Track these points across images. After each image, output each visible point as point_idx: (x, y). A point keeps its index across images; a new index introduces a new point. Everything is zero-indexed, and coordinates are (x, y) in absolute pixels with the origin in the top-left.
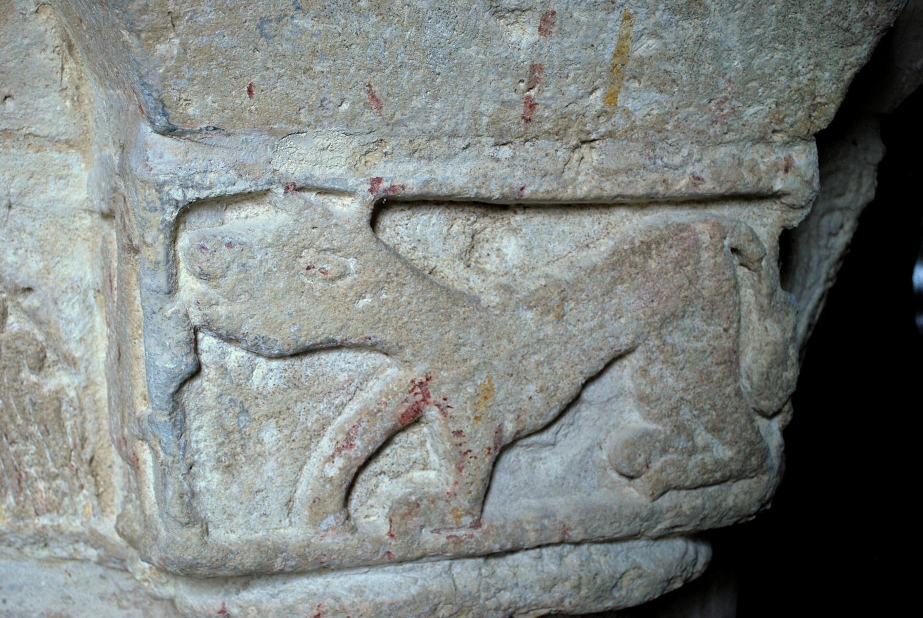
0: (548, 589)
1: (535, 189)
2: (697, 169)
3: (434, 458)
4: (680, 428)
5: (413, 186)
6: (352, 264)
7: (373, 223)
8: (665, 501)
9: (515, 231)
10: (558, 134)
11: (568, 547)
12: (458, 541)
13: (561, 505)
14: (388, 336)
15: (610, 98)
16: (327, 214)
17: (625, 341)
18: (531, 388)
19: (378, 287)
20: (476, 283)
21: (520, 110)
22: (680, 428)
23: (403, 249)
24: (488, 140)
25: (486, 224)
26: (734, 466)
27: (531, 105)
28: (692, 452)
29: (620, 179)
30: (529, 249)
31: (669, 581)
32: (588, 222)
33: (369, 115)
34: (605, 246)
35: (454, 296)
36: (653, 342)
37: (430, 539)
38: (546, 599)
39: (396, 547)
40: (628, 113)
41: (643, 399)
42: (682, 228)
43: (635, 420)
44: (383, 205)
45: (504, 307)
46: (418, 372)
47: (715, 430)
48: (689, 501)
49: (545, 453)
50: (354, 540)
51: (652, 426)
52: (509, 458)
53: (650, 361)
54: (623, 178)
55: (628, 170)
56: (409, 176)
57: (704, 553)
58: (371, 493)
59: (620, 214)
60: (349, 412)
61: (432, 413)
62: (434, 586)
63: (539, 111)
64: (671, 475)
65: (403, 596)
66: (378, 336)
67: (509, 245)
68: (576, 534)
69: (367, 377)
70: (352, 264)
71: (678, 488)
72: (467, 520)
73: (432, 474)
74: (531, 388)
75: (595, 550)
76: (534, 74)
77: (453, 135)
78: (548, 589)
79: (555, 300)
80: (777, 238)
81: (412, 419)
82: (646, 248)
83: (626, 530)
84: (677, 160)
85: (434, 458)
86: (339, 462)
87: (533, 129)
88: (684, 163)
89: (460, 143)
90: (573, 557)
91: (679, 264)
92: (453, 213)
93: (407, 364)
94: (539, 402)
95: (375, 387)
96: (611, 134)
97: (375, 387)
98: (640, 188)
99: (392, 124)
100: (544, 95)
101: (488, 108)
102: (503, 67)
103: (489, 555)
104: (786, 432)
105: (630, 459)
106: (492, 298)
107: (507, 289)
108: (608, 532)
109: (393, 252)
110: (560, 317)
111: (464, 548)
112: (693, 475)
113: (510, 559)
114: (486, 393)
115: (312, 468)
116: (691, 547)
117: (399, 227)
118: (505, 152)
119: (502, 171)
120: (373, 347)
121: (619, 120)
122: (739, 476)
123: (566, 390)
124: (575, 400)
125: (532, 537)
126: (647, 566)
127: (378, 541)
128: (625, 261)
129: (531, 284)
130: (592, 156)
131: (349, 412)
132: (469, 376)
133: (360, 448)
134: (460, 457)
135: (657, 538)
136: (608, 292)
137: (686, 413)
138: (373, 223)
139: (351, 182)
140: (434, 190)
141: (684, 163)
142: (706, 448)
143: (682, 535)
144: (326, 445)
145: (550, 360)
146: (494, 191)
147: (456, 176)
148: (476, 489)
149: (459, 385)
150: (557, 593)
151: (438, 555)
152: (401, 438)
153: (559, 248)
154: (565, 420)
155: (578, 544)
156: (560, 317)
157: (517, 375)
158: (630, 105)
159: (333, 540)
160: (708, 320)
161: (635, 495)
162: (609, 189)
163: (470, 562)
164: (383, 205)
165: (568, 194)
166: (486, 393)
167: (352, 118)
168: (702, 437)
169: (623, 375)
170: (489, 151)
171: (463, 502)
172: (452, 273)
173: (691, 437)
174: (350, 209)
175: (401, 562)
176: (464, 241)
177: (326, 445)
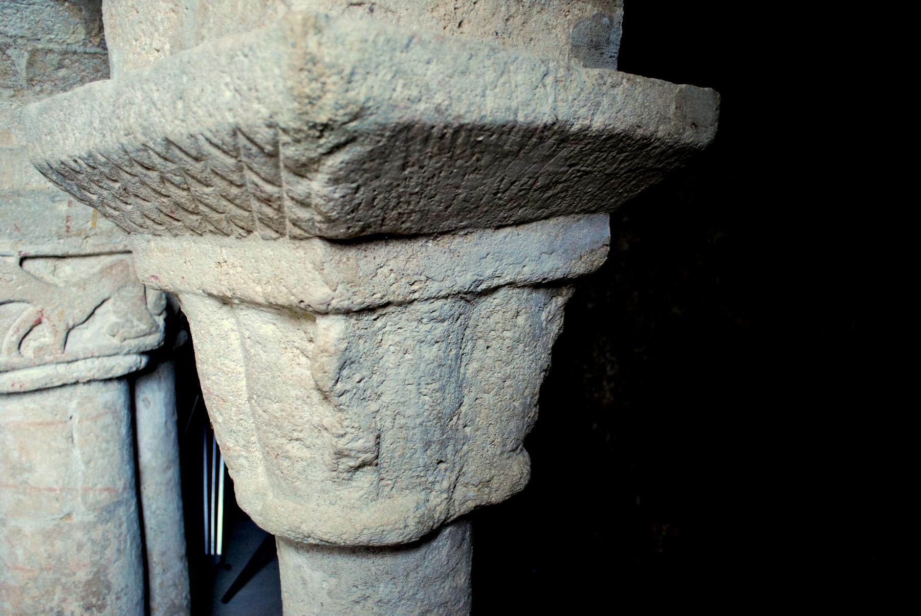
0: (90, 371)
1: (72, 252)
2: (125, 243)
3: (47, 334)
4: (127, 320)
5: (32, 253)
6: (14, 277)
7: (21, 264)
8: (126, 343)
9: (69, 264)
10: (78, 235)
11: (95, 359)
12: (57, 358)
13: (90, 346)
14: (28, 298)
15: (94, 224)
16: (5, 262)
17: (106, 296)
18: (77, 311)
19: (23, 283)
20: (56, 280)
21: (65, 229)
22: (127, 320)
23: (32, 272)
24: (55, 238)
25: (59, 263)
26: (147, 331)
27: (68, 227)
28: (133, 327)
29: (562, 70)
30: (73, 269)
31: (131, 368)
32: (92, 260)
33: (16, 233)
34: (99, 267)
35: (48, 284)
36: (116, 295)
37: (48, 358)
38: (89, 375)
39: (37, 361)
40: (100, 228)
41: (115, 312)
42: (122, 261)
43: (113, 319)
44: (22, 260)
45: (65, 287)
46: (39, 308)
47: (140, 320)
48: (134, 343)
49: (85, 331)
50: (22, 360)
51: (118, 320)
52: (72, 333)
53: (116, 301)
54: (101, 247)
55: (102, 244)
56: (31, 250)
57: (144, 360)
58: (27, 346)
59: (102, 257)
60: (18, 321)
61: (44, 320)
62: (51, 372)
63: (71, 229)
64: (126, 335)
65: (41, 376)
66: (24, 298)
67: (67, 268)
68: (97, 354)
69: (23, 311)
70: (14, 277)
71: (129, 338)
72: (60, 351)
73: (47, 339)
74: (77, 311)
75: (105, 359)
76: (68, 218)
77: (44, 237)
78: (90, 371)
79: (82, 284)
80: (334, 249)
81: (39, 322)
82: (111, 267)
83: (113, 352)
84: (119, 240)
85: (47, 334)
86: (15, 336)
87: (70, 234)
88: (121, 241)
89: (46, 239)
90: (97, 362)
91: (122, 271)
92: (48, 260)
93: (35, 306)
94: (80, 315)
95: (25, 314)
96: (96, 234)
97: (25, 314)
98: (107, 249)
99: (24, 235)
100: (72, 224)
101: (54, 229)
102: (58, 217)
103: (69, 362)
104: (166, 320)
105: (112, 331)
106: (62, 285)
107: (67, 282)
108: (107, 353)
109: (28, 273)
110: (84, 289)
111: (60, 360)
112: (133, 334)
113: (76, 364)
114: (62, 313)
115: (7, 339)
116: (139, 358)
117: (28, 264)
118: (62, 241)
119: (61, 247)
120: (24, 301)
121: (98, 230)
122: (150, 334)
123: (89, 311)
124: (93, 313)
125: (82, 356)
126: (122, 363)
127: (31, 360)
128: (105, 271)
129: (74, 280)
130: (90, 241)
131: (18, 321)
132: (56, 308)
133: (22, 332)
134: (55, 333)
135: (126, 355)
136: (100, 280)
137: (129, 316)
138: (21, 264)
139: (12, 253)
140: (39, 254)
141: (121, 241)
142: (137, 326)
143: (134, 353)
144: (11, 332)
145: (82, 302)
146: (59, 253)
147: (47, 249)
148: (62, 342)
149: (53, 310)
150: (92, 373)
151: (51, 363)
152: (35, 328)
153: (83, 269)
154: (90, 320)
155: (98, 357)
156: (84, 289)
157: (71, 307)
158: (100, 225)
159: (15, 359)
160: (134, 287)
161: (116, 341)
162: (97, 250)
163: (62, 365)
164: (22, 260)
165: (83, 252)
166: (62, 313)
167: (10, 234)
168: (136, 323)
169: (107, 306)
170: (56, 241)
171: (58, 346)
172: (49, 278)
173: (132, 322)
174: (14, 260)
175: (39, 365)
176: (52, 268)
177: (11, 332)
